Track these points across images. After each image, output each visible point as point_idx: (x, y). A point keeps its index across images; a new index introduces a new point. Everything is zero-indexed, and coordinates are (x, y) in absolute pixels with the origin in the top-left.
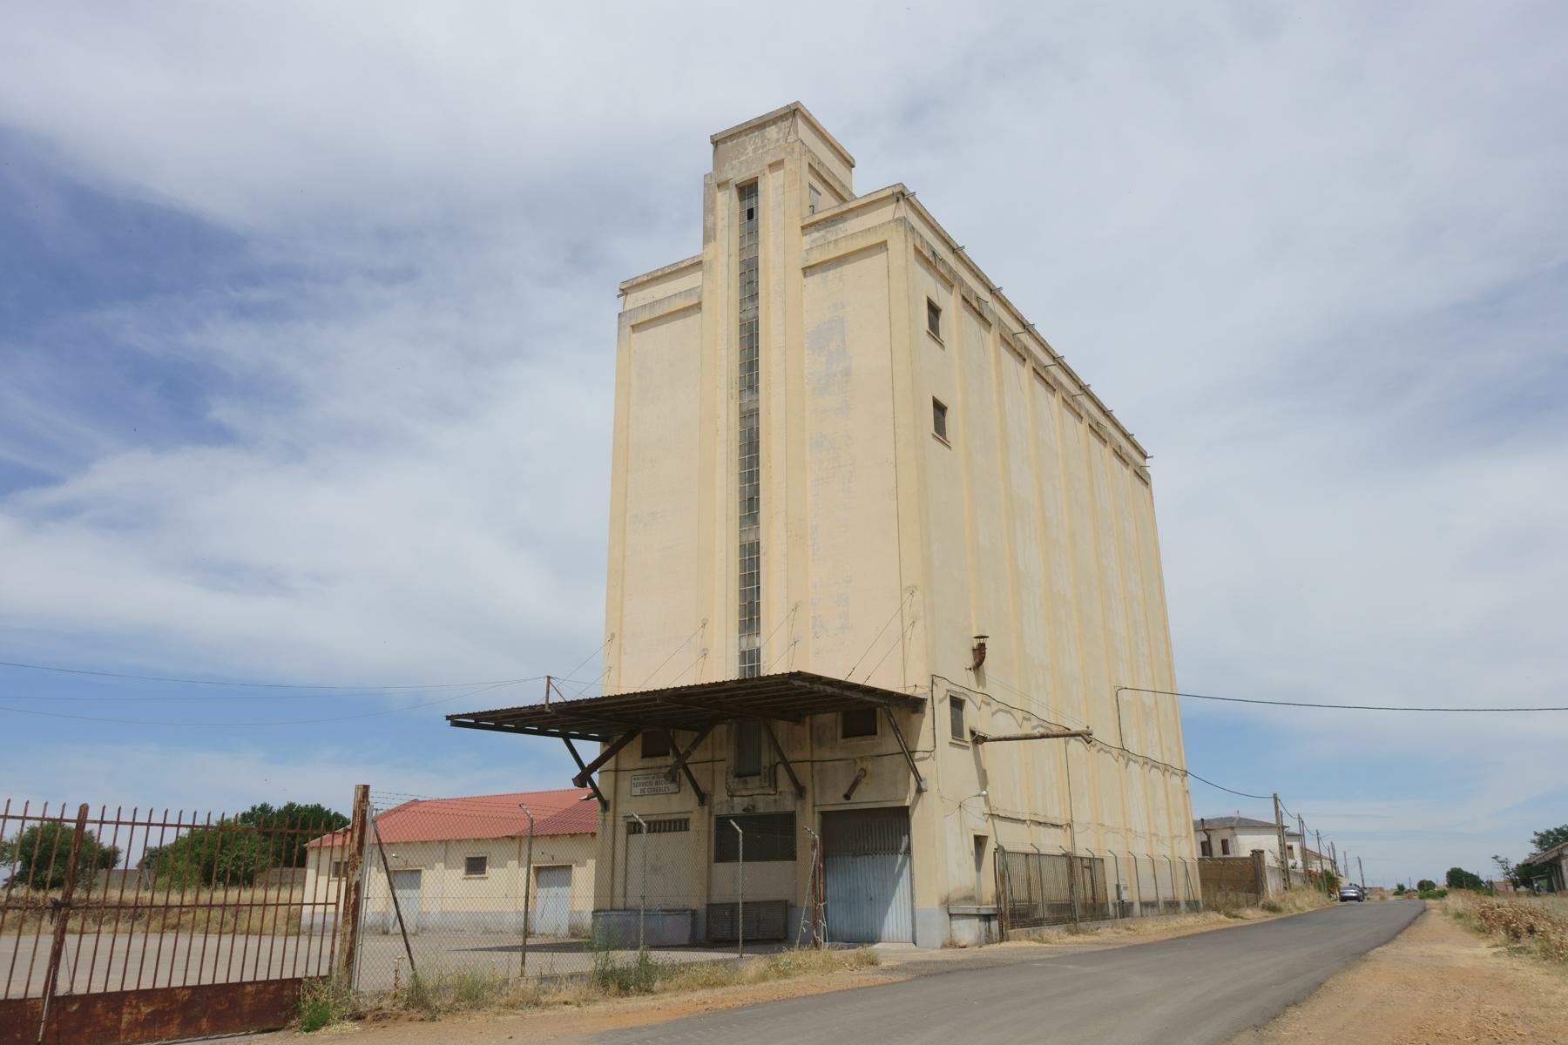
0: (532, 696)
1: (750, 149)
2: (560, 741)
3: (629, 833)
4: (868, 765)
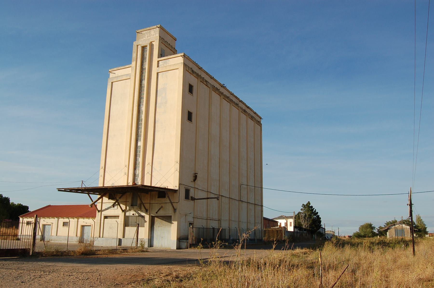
0: (78, 185)
1: (146, 36)
2: (87, 195)
3: (104, 219)
4: (163, 205)
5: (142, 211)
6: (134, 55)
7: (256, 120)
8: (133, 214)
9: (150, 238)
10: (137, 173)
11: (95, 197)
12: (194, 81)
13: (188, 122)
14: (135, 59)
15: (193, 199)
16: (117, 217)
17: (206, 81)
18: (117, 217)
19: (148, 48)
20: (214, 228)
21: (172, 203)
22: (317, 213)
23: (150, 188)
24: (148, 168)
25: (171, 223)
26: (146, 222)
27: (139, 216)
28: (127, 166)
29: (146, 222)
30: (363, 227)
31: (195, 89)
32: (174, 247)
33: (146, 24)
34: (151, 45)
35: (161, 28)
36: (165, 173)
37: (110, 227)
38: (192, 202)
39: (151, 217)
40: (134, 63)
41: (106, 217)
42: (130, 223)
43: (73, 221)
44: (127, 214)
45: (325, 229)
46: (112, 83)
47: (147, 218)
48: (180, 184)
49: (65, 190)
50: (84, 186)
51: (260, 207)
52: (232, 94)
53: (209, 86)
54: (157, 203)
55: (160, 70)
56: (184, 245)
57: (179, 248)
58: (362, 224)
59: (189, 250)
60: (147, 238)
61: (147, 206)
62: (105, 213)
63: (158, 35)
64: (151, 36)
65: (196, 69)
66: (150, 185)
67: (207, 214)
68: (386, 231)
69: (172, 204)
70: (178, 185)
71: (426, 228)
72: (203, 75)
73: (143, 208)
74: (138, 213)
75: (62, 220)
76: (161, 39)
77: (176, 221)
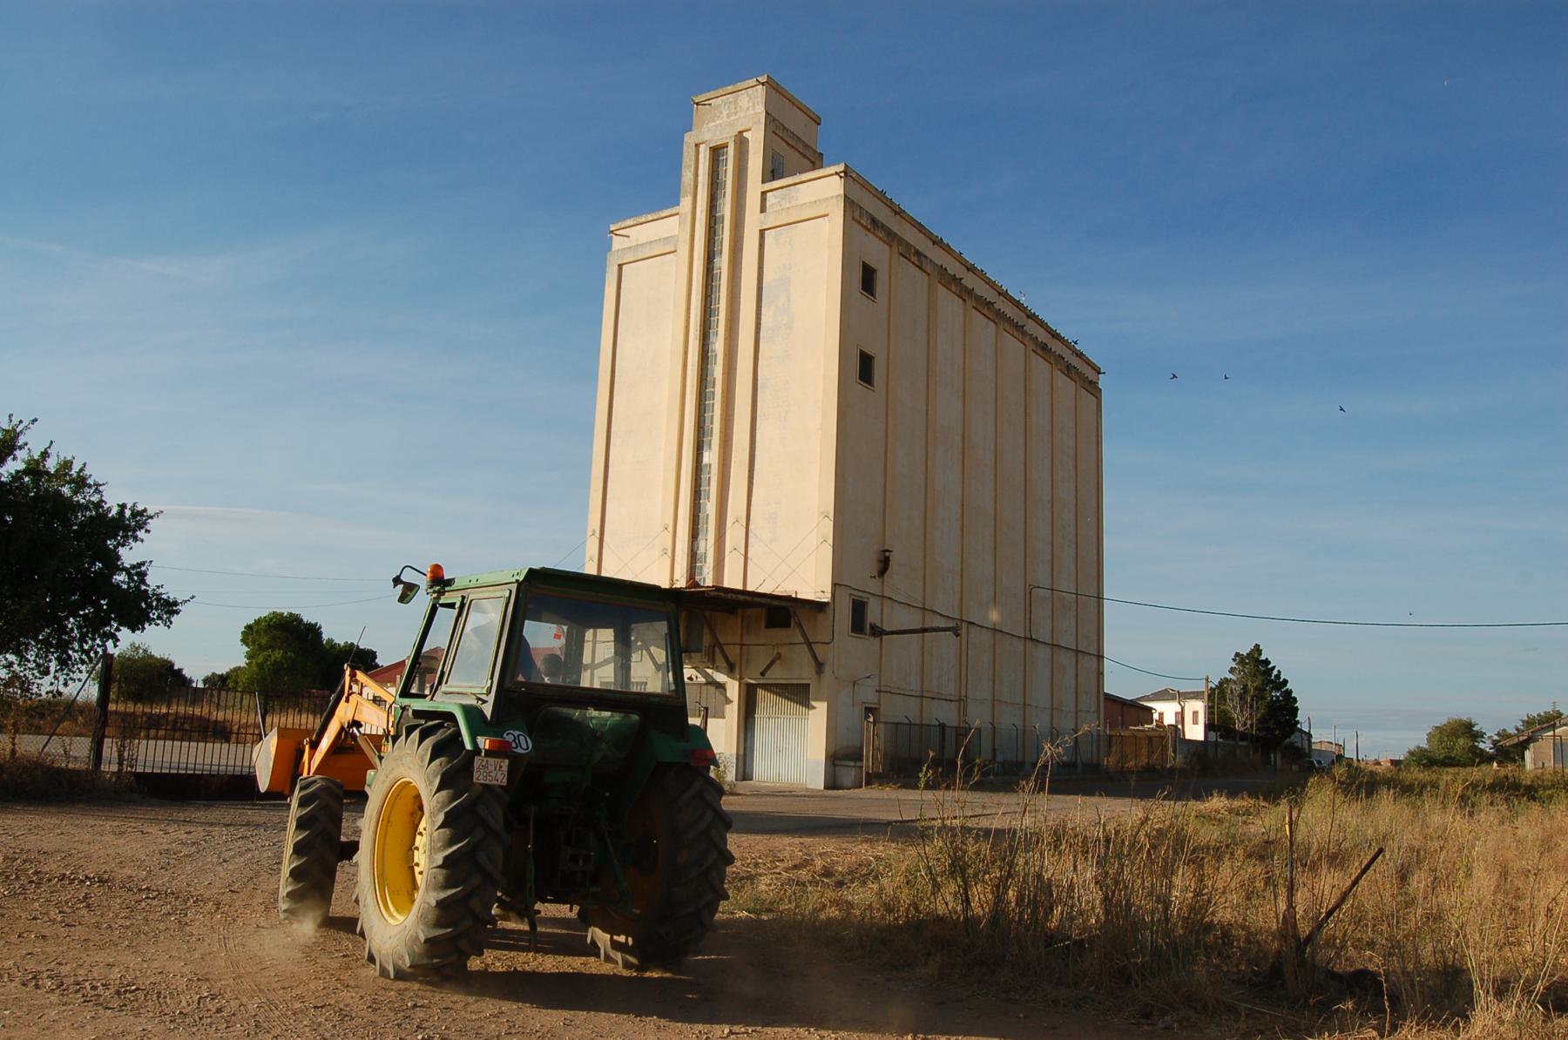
4: (782, 650)
5: (717, 669)
6: (687, 177)
7: (1082, 375)
10: (701, 550)
13: (859, 388)
15: (877, 632)
17: (918, 253)
19: (731, 151)
20: (942, 726)
21: (810, 645)
22: (1285, 682)
23: (741, 597)
24: (734, 535)
25: (809, 707)
26: (729, 701)
27: (708, 683)
28: (670, 529)
29: (729, 701)
33: (726, 75)
34: (741, 142)
35: (772, 86)
36: (788, 550)
40: (686, 203)
45: (1310, 735)
46: (620, 266)
47: (733, 689)
48: (835, 585)
52: (1004, 294)
57: (832, 783)
58: (1441, 721)
64: (738, 113)
65: (883, 215)
69: (811, 649)
70: (829, 589)
72: (910, 235)
73: (720, 661)
74: (706, 675)
76: (774, 125)
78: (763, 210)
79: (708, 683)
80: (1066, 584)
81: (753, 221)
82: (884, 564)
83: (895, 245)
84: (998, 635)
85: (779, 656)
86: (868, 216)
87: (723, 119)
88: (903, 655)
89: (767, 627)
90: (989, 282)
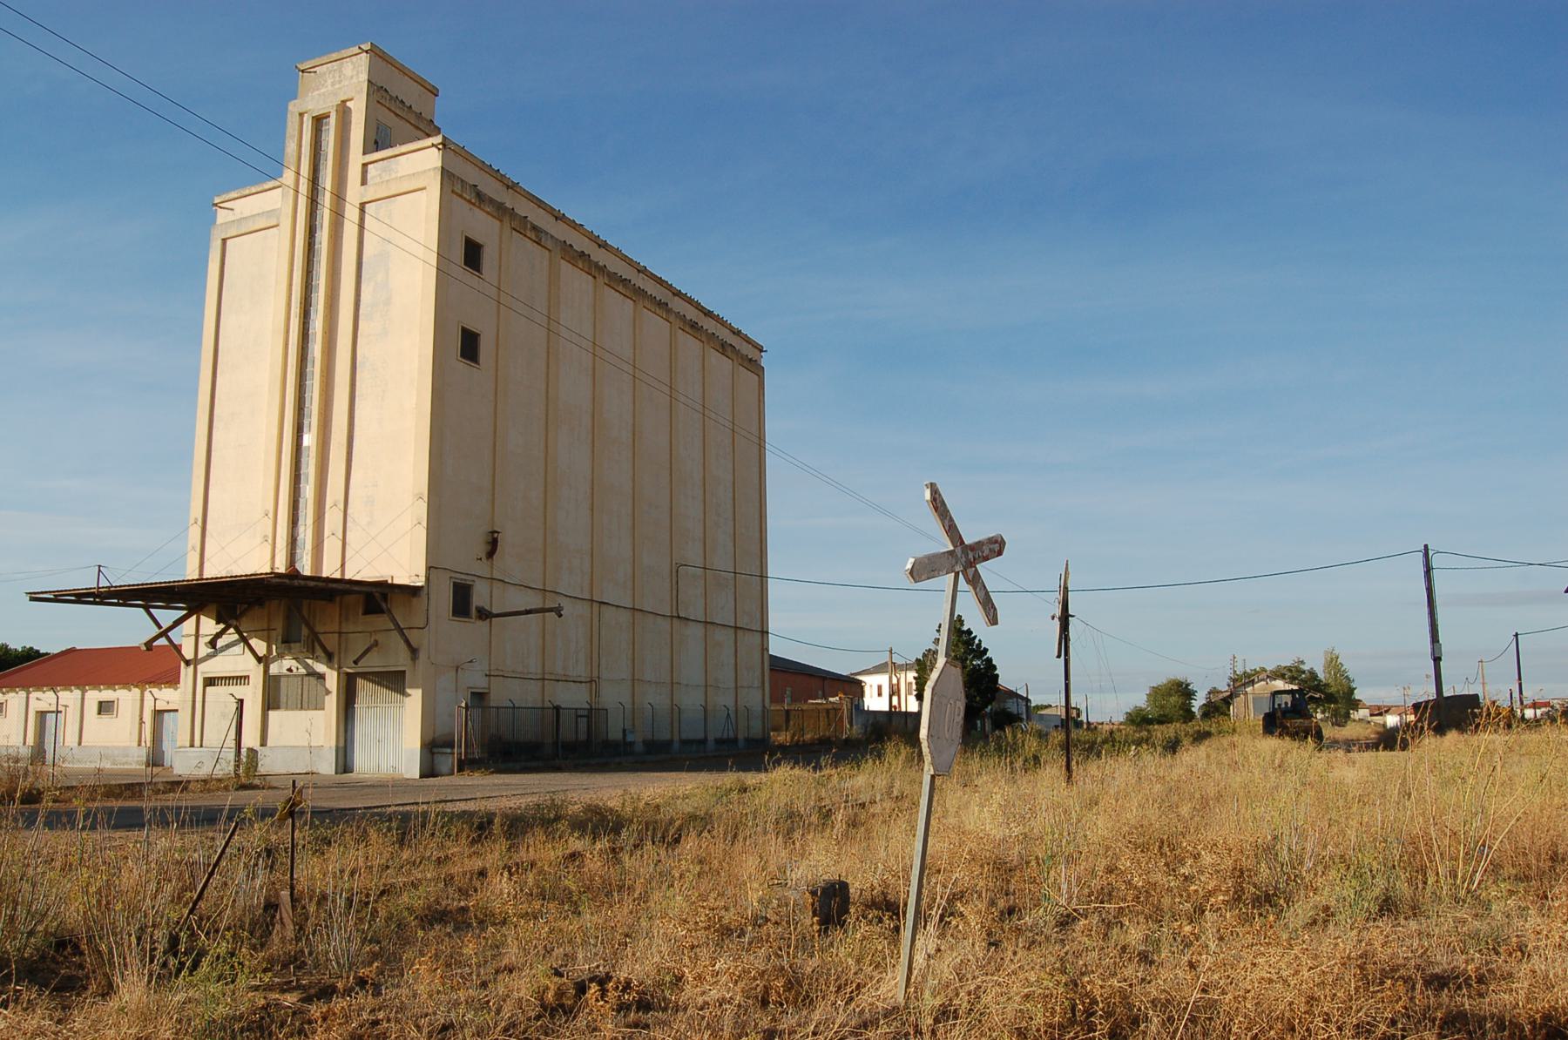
0: (87, 582)
4: (379, 637)
5: (317, 659)
6: (291, 147)
7: (744, 356)
8: (290, 670)
9: (342, 744)
10: (301, 537)
11: (166, 616)
12: (484, 227)
13: (462, 366)
14: (293, 160)
15: (484, 615)
16: (242, 679)
17: (534, 228)
18: (242, 679)
19: (333, 120)
20: (557, 709)
21: (401, 631)
22: (986, 650)
23: (312, 584)
24: (332, 519)
25: (404, 694)
26: (328, 692)
27: (308, 675)
28: (271, 515)
29: (328, 692)
30: (1157, 693)
31: (488, 258)
32: (415, 772)
33: (330, 43)
34: (344, 111)
35: (376, 53)
36: (384, 538)
37: (229, 712)
38: (483, 626)
39: (344, 677)
40: (288, 177)
41: (210, 682)
42: (283, 699)
43: (126, 698)
44: (274, 669)
45: (1028, 700)
46: (224, 241)
47: (332, 679)
48: (429, 568)
49: (59, 597)
50: (104, 583)
51: (758, 636)
52: (643, 271)
53: (549, 244)
54: (361, 629)
55: (370, 193)
56: (447, 761)
57: (429, 771)
58: (1161, 680)
59: (457, 780)
60: (333, 743)
61: (331, 642)
62: (207, 669)
63: (364, 77)
64: (343, 82)
65: (491, 188)
66: (337, 575)
67: (533, 666)
68: (1227, 701)
69: (403, 635)
70: (423, 572)
71: (1352, 691)
72: (524, 209)
73: (319, 652)
74: (307, 666)
75: (94, 696)
76: (377, 91)
77: (417, 687)
78: (364, 182)
79: (308, 675)
80: (722, 561)
81: (354, 193)
82: (493, 545)
83: (506, 219)
84: (638, 614)
85: (376, 644)
86: (463, 185)
87: (328, 87)
88: (518, 643)
89: (366, 612)
90: (625, 259)
